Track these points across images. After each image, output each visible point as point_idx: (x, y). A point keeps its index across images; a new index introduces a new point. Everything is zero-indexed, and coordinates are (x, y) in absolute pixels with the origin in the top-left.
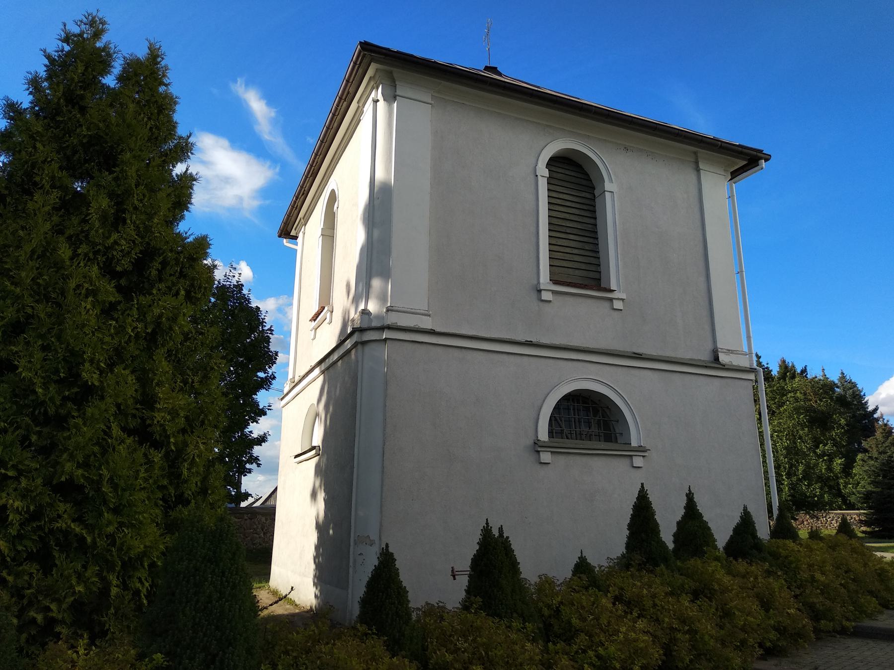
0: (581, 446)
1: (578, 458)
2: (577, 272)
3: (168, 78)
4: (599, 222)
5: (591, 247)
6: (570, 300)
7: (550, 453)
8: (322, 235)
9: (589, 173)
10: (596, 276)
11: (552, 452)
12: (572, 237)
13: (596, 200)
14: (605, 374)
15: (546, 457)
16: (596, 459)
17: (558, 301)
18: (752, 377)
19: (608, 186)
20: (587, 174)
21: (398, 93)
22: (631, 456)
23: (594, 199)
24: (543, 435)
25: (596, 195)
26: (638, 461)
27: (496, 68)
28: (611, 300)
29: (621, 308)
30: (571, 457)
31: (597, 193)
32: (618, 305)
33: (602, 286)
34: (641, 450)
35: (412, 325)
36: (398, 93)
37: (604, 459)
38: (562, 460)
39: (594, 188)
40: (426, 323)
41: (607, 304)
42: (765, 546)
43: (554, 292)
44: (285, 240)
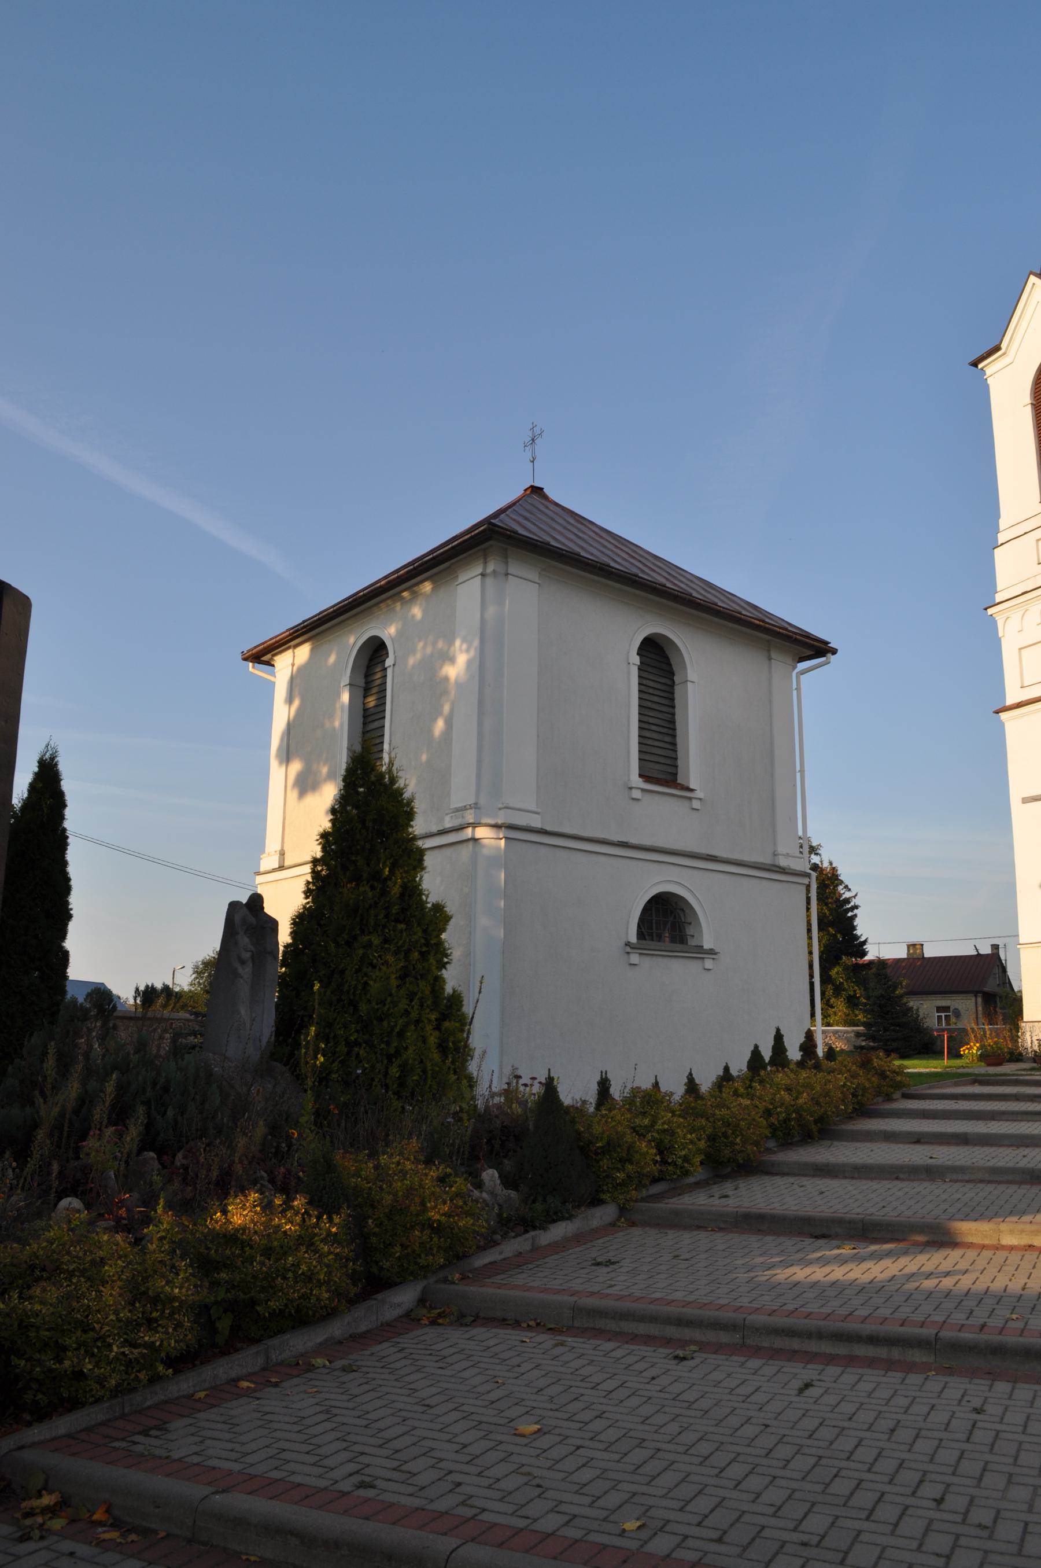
0: (663, 948)
1: (660, 959)
2: (657, 767)
3: (846, 887)
4: (678, 711)
5: (668, 739)
6: (657, 797)
7: (637, 955)
8: (350, 684)
9: (669, 656)
10: (671, 770)
11: (640, 954)
12: (654, 728)
13: (676, 687)
14: (673, 874)
15: (635, 958)
16: (674, 960)
17: (647, 798)
18: (806, 881)
19: (691, 675)
20: (668, 658)
21: (511, 570)
22: (703, 958)
23: (672, 685)
24: (633, 939)
25: (677, 682)
26: (709, 963)
27: (541, 489)
28: (690, 799)
29: (698, 807)
30: (654, 958)
31: (677, 679)
32: (696, 804)
33: (679, 781)
34: (712, 952)
35: (525, 824)
36: (510, 571)
37: (681, 960)
38: (647, 963)
39: (673, 674)
40: (536, 822)
41: (686, 803)
42: (499, 1106)
43: (643, 790)
44: (251, 664)
